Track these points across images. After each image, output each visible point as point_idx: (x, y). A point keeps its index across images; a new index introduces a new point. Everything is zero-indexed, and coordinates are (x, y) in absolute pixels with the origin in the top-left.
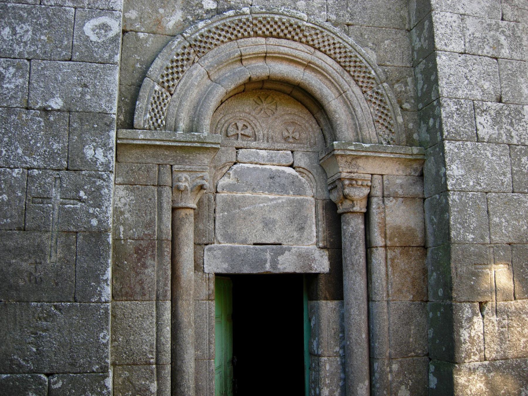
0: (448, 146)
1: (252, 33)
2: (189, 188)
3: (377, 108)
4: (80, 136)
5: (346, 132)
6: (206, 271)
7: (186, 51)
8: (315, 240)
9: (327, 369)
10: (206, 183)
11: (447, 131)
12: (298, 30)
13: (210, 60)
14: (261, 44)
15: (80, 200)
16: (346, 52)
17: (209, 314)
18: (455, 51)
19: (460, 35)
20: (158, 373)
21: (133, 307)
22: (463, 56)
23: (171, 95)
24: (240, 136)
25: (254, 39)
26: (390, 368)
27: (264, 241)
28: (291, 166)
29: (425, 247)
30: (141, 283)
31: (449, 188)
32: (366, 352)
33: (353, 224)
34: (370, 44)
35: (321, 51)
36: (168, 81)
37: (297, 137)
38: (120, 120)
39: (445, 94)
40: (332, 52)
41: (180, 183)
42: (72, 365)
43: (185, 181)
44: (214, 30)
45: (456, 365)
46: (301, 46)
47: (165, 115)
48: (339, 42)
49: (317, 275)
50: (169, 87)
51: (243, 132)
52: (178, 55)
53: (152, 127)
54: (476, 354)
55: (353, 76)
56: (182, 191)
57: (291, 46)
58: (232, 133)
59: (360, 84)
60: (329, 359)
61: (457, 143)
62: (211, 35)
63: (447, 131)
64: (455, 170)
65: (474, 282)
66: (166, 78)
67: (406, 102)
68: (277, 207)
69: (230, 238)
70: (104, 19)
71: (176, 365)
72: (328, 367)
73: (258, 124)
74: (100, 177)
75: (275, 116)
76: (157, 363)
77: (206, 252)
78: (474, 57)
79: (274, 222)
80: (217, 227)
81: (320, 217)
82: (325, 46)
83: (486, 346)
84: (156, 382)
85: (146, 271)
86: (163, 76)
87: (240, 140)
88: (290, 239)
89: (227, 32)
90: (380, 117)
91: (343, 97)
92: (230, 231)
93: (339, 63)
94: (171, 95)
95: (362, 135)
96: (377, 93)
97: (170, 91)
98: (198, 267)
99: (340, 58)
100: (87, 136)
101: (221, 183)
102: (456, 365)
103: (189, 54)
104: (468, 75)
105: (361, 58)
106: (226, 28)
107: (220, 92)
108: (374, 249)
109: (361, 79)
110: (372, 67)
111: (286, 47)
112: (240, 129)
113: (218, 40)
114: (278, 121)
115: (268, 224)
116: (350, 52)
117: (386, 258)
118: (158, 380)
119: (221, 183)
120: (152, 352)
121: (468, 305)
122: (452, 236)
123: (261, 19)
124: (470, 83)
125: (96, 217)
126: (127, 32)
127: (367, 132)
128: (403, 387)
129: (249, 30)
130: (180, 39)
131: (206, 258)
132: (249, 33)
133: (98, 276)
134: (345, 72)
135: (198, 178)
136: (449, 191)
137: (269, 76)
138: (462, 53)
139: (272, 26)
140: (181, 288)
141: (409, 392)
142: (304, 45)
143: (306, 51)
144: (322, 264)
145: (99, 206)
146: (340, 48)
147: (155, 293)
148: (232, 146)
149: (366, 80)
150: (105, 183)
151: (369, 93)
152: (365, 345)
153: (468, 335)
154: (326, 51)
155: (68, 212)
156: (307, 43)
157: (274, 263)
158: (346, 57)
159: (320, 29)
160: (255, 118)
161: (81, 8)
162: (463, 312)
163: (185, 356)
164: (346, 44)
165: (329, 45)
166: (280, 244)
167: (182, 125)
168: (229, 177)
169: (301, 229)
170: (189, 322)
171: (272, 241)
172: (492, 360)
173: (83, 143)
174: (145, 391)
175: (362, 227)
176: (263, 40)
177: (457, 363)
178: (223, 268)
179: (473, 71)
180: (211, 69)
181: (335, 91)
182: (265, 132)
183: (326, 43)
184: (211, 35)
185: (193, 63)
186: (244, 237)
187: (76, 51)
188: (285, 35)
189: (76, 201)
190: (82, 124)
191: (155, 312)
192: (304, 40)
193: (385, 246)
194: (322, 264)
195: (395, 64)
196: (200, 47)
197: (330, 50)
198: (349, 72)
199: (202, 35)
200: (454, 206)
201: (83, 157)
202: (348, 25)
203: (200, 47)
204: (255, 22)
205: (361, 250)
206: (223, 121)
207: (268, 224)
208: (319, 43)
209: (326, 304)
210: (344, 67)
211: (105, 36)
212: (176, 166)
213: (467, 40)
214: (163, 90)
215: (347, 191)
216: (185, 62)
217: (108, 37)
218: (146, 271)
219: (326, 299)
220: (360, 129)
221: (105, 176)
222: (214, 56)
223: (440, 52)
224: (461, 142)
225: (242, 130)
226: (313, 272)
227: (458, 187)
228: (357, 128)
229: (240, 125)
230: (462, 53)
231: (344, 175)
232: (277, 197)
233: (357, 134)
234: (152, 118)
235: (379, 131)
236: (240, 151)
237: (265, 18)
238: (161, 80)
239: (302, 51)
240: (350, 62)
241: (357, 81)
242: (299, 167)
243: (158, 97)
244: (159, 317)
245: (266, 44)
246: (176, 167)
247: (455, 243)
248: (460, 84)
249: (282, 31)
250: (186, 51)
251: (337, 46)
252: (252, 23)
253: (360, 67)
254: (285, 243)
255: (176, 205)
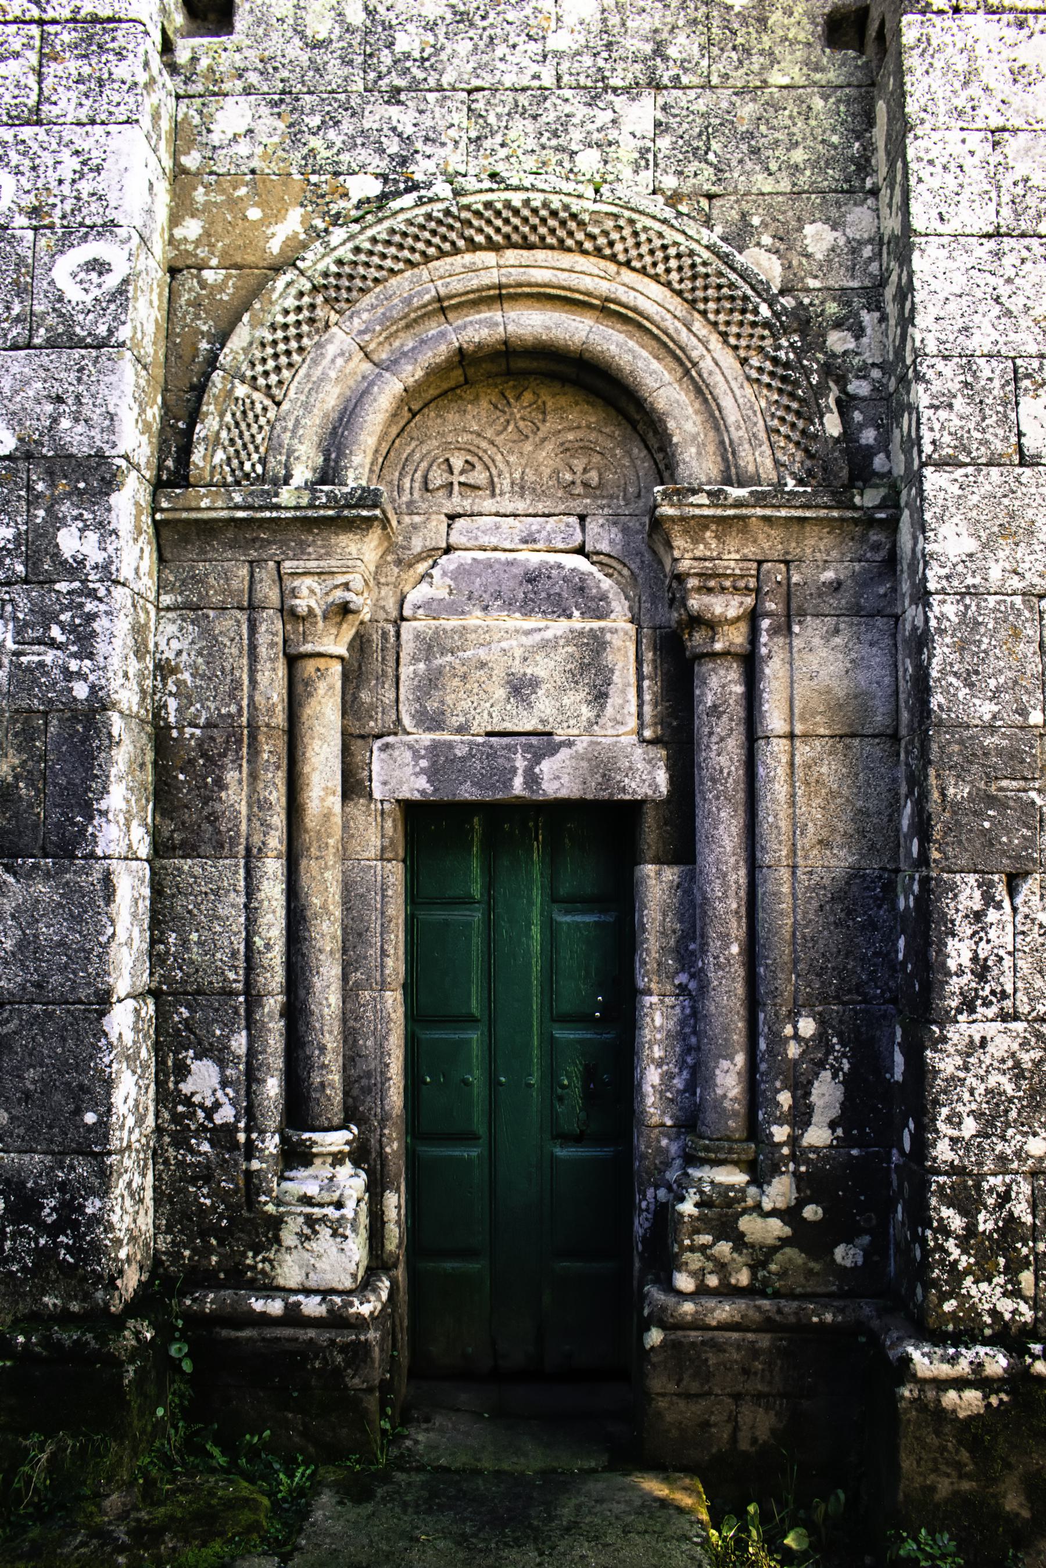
0: (933, 480)
1: (461, 243)
2: (318, 612)
3: (776, 397)
4: (49, 510)
5: (697, 463)
6: (377, 795)
7: (306, 300)
8: (632, 723)
9: (658, 1023)
10: (354, 598)
11: (934, 442)
12: (572, 225)
13: (365, 316)
14: (489, 268)
15: (53, 644)
16: (693, 266)
17: (383, 890)
18: (968, 231)
19: (988, 188)
20: (249, 1013)
21: (198, 871)
22: (991, 244)
23: (278, 404)
24: (456, 487)
25: (468, 258)
26: (795, 1028)
27: (509, 727)
28: (580, 551)
29: (894, 737)
30: (213, 819)
31: (932, 586)
32: (739, 988)
33: (714, 682)
34: (766, 240)
35: (634, 269)
36: (266, 374)
37: (595, 482)
38: (168, 468)
39: (931, 348)
40: (661, 268)
41: (297, 602)
42: (38, 986)
43: (309, 596)
44: (367, 245)
45: (934, 1028)
46: (581, 262)
47: (262, 449)
48: (676, 244)
49: (636, 807)
50: (269, 387)
51: (462, 479)
52: (286, 312)
53: (230, 479)
54: (991, 1003)
55: (715, 324)
56: (304, 619)
57: (558, 265)
58: (439, 482)
59: (732, 341)
60: (662, 1002)
61: (962, 471)
62: (363, 257)
63: (934, 442)
64: (950, 541)
65: (993, 824)
66: (259, 368)
67: (858, 377)
68: (544, 646)
69: (432, 721)
70: (92, 249)
71: (297, 997)
72: (658, 1021)
73: (499, 458)
74: (93, 594)
75: (541, 434)
76: (247, 992)
77: (376, 753)
78: (1026, 241)
79: (534, 683)
80: (402, 698)
81: (647, 669)
82: (641, 256)
83: (1020, 985)
84: (244, 1033)
85: (223, 794)
86: (253, 365)
87: (456, 499)
88: (572, 722)
89: (401, 247)
90: (782, 420)
91: (692, 378)
92: (432, 705)
93: (679, 293)
94: (278, 404)
95: (737, 466)
96: (775, 361)
97: (272, 397)
98: (353, 785)
99: (681, 281)
100: (65, 508)
101: (417, 595)
102: (934, 1028)
103: (313, 307)
104: (1004, 291)
105: (733, 277)
106: (397, 238)
107: (389, 391)
108: (762, 742)
109: (734, 329)
110: (759, 295)
111: (544, 267)
112: (456, 472)
113: (380, 268)
114: (549, 446)
115: (521, 689)
116: (705, 264)
117: (792, 764)
118: (248, 1028)
119: (417, 595)
120: (235, 967)
121: (972, 879)
122: (934, 705)
123: (480, 207)
124: (1009, 313)
125: (86, 680)
126: (180, 271)
127: (750, 458)
128: (826, 1075)
129: (453, 235)
130: (290, 275)
131: (376, 767)
132: (453, 243)
133: (88, 804)
134: (696, 315)
135: (336, 587)
136: (931, 594)
137: (505, 343)
138: (988, 236)
139: (507, 221)
140: (306, 831)
141: (841, 1088)
142: (592, 259)
143: (596, 271)
144: (648, 777)
145: (91, 656)
146: (679, 256)
147: (243, 840)
148: (438, 513)
149: (747, 330)
150: (103, 607)
151: (755, 362)
152: (739, 971)
153: (970, 955)
154: (644, 267)
155: (29, 669)
156: (598, 251)
157: (532, 779)
158: (694, 277)
159: (627, 214)
160: (492, 443)
161: (45, 227)
162: (956, 896)
163: (315, 979)
164: (694, 246)
165: (652, 252)
166: (550, 734)
167: (301, 474)
168: (431, 584)
169: (599, 697)
170: (324, 907)
171: (529, 728)
172: (1035, 1020)
173: (56, 522)
174: (220, 1051)
175: (739, 689)
176: (489, 258)
177: (935, 1022)
178: (415, 785)
179: (1017, 281)
180: (367, 337)
181: (674, 365)
182: (517, 476)
183: (644, 249)
184: (363, 257)
185: (327, 326)
186: (462, 719)
187: (39, 326)
188: (543, 238)
189: (42, 648)
190: (53, 485)
191: (242, 883)
192: (588, 245)
193: (791, 736)
194: (648, 777)
195: (831, 283)
196: (338, 288)
197: (655, 264)
198: (704, 313)
199: (340, 262)
200: (942, 632)
201: (56, 554)
202: (710, 197)
203: (339, 290)
204: (465, 215)
205: (734, 745)
206: (417, 456)
207: (521, 689)
208: (626, 251)
209: (658, 873)
210: (692, 303)
211: (99, 286)
212: (287, 564)
213: (1006, 198)
214: (257, 396)
215: (695, 603)
216: (305, 328)
217: (105, 288)
218: (223, 794)
219: (658, 861)
220: (734, 453)
221: (102, 592)
222: (373, 307)
223: (923, 240)
224: (970, 470)
225: (462, 473)
226: (628, 797)
227: (955, 583)
228: (727, 452)
229: (458, 463)
230: (988, 236)
231: (685, 565)
232: (542, 624)
233: (728, 468)
234: (229, 459)
235: (779, 455)
236: (459, 523)
237: (488, 205)
238: (249, 373)
239: (588, 274)
240: (706, 288)
241: (724, 335)
242: (598, 553)
243: (244, 412)
244: (251, 891)
245: (499, 266)
246: (288, 566)
247: (940, 723)
248: (977, 318)
249: (534, 228)
250: (306, 300)
251: (672, 251)
252: (457, 218)
253: (732, 298)
254: (559, 731)
255: (292, 651)
